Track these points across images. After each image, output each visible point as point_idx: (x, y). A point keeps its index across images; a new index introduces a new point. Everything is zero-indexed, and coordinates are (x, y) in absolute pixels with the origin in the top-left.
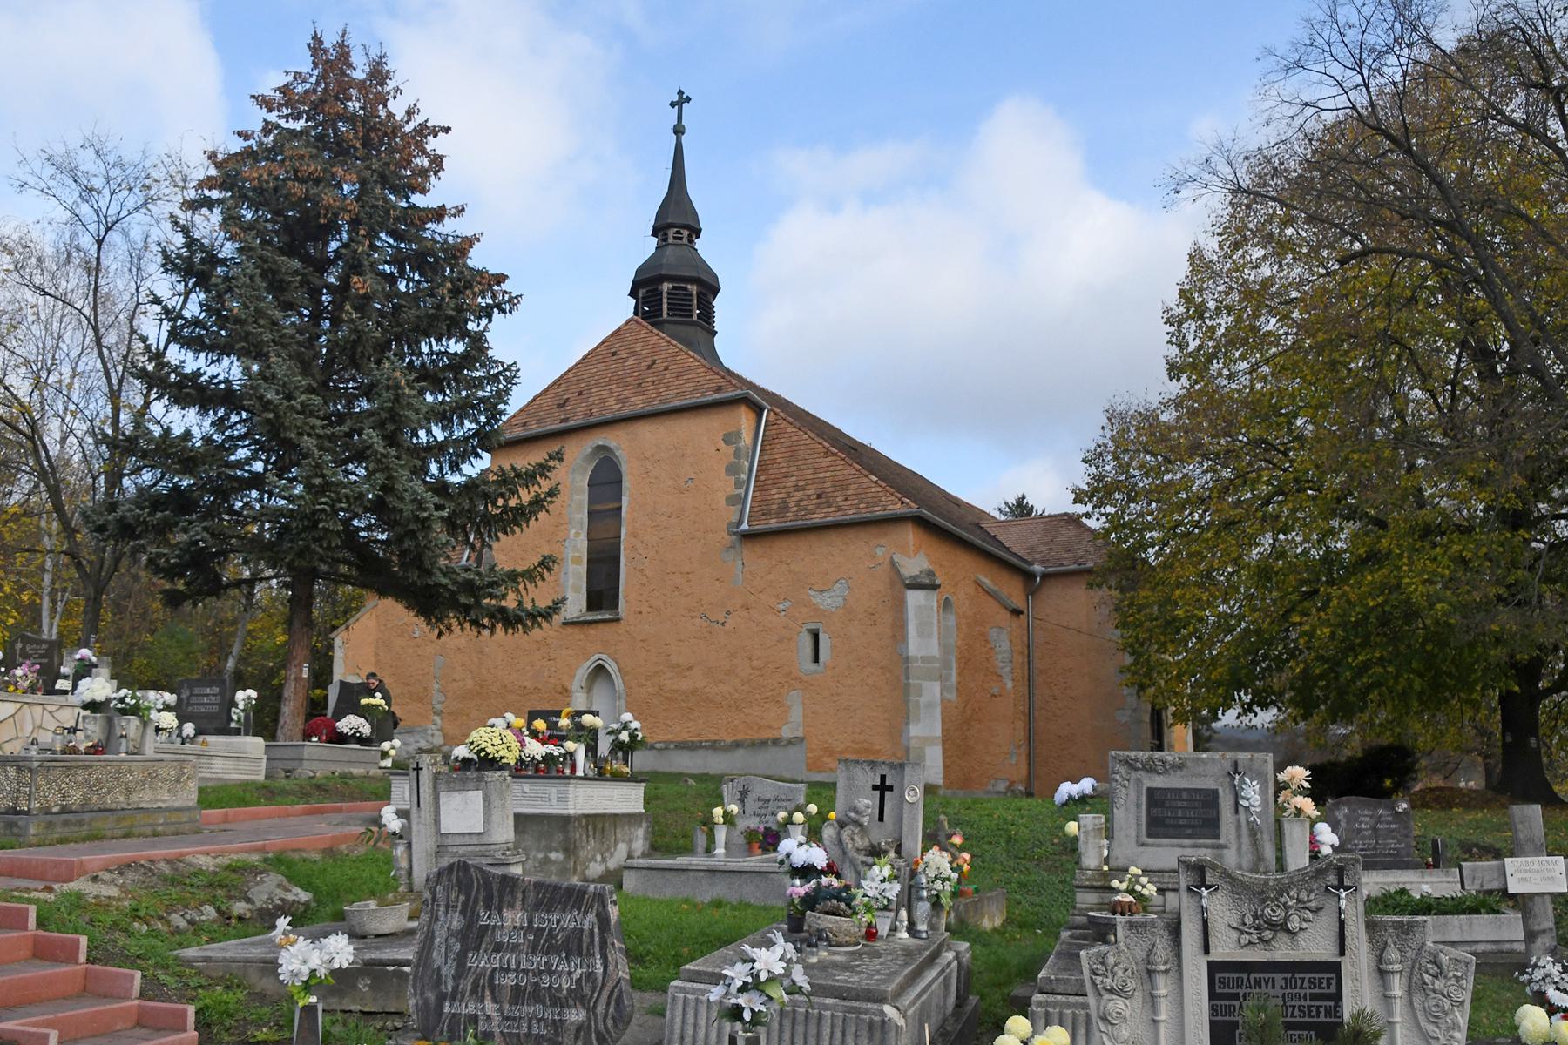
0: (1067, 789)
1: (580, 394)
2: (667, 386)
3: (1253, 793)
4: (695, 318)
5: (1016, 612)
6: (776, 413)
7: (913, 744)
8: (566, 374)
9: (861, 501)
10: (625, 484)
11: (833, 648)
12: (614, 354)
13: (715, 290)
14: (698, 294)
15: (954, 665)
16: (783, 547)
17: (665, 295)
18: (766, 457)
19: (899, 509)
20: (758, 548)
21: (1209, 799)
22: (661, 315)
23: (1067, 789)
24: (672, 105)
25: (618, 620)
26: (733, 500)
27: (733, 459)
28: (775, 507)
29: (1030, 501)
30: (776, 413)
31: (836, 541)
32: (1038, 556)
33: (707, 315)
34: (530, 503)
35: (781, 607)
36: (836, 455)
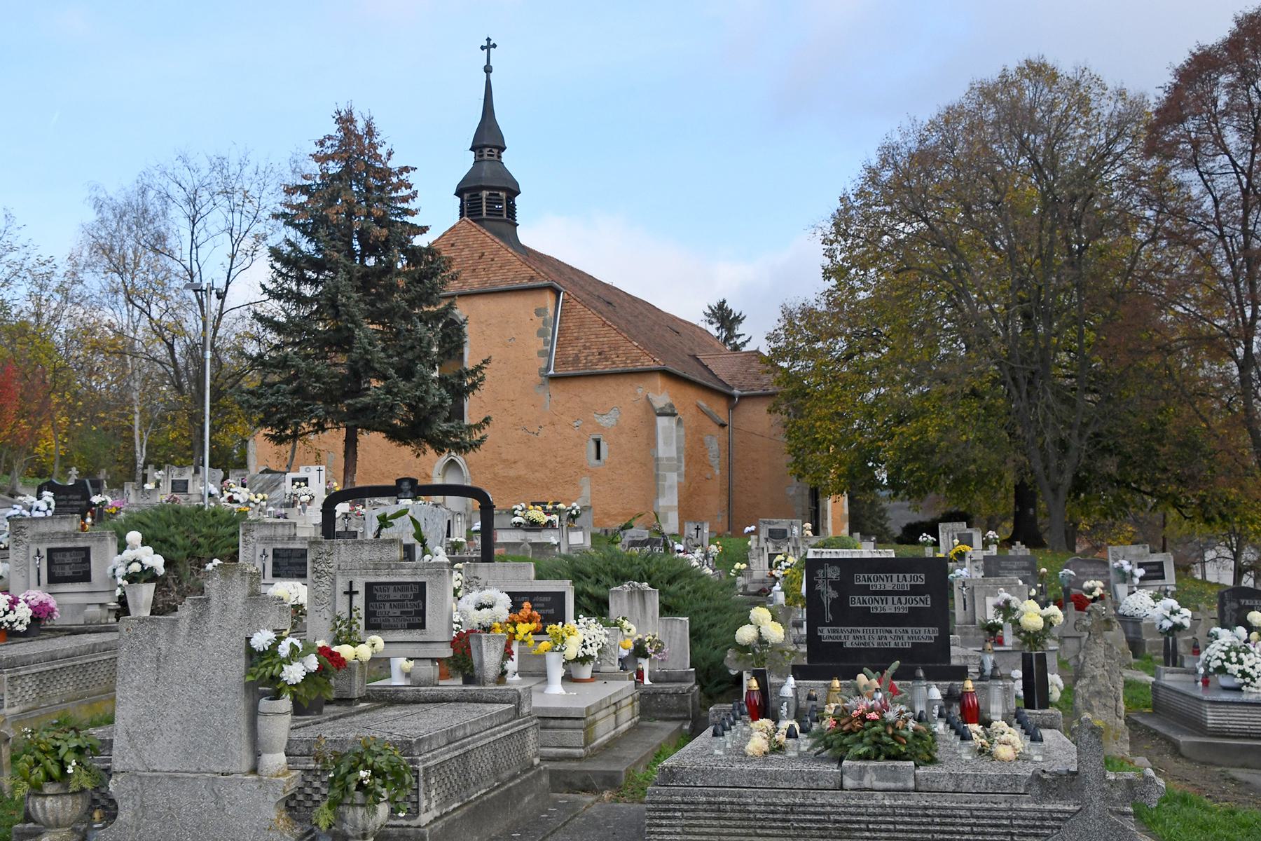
0: (748, 529)
3: (796, 530)
4: (505, 216)
5: (723, 425)
7: (661, 510)
9: (627, 359)
11: (610, 450)
12: (453, 245)
15: (683, 460)
16: (576, 386)
17: (484, 200)
19: (653, 365)
20: (560, 386)
21: (785, 532)
23: (748, 529)
26: (541, 353)
29: (729, 305)
31: (611, 384)
32: (736, 383)
33: (511, 211)
35: (576, 424)
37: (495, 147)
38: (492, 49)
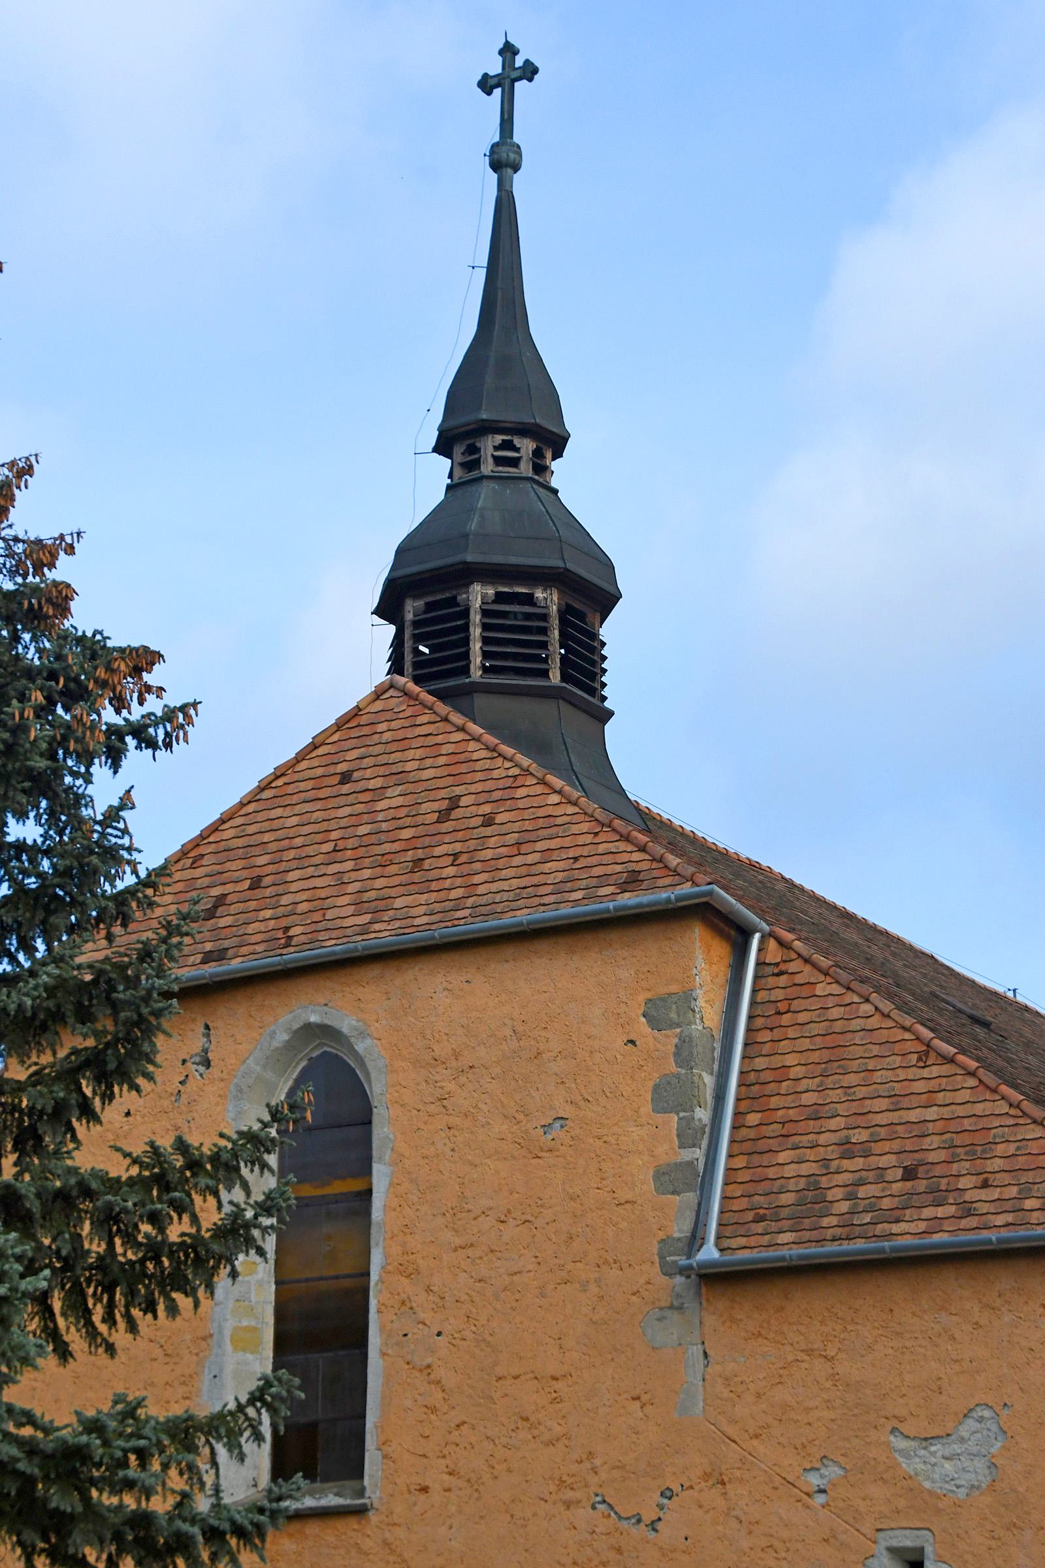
1: (256, 884)
2: (493, 868)
4: (555, 677)
6: (781, 943)
8: (215, 828)
10: (382, 1131)
12: (346, 778)
13: (607, 600)
14: (566, 613)
17: (476, 618)
18: (760, 1063)
22: (466, 671)
24: (486, 85)
25: (360, 1511)
27: (672, 1067)
28: (787, 1198)
30: (781, 943)
34: (220, 1232)
35: (814, 1480)
36: (951, 1060)
37: (524, 431)
38: (521, 87)
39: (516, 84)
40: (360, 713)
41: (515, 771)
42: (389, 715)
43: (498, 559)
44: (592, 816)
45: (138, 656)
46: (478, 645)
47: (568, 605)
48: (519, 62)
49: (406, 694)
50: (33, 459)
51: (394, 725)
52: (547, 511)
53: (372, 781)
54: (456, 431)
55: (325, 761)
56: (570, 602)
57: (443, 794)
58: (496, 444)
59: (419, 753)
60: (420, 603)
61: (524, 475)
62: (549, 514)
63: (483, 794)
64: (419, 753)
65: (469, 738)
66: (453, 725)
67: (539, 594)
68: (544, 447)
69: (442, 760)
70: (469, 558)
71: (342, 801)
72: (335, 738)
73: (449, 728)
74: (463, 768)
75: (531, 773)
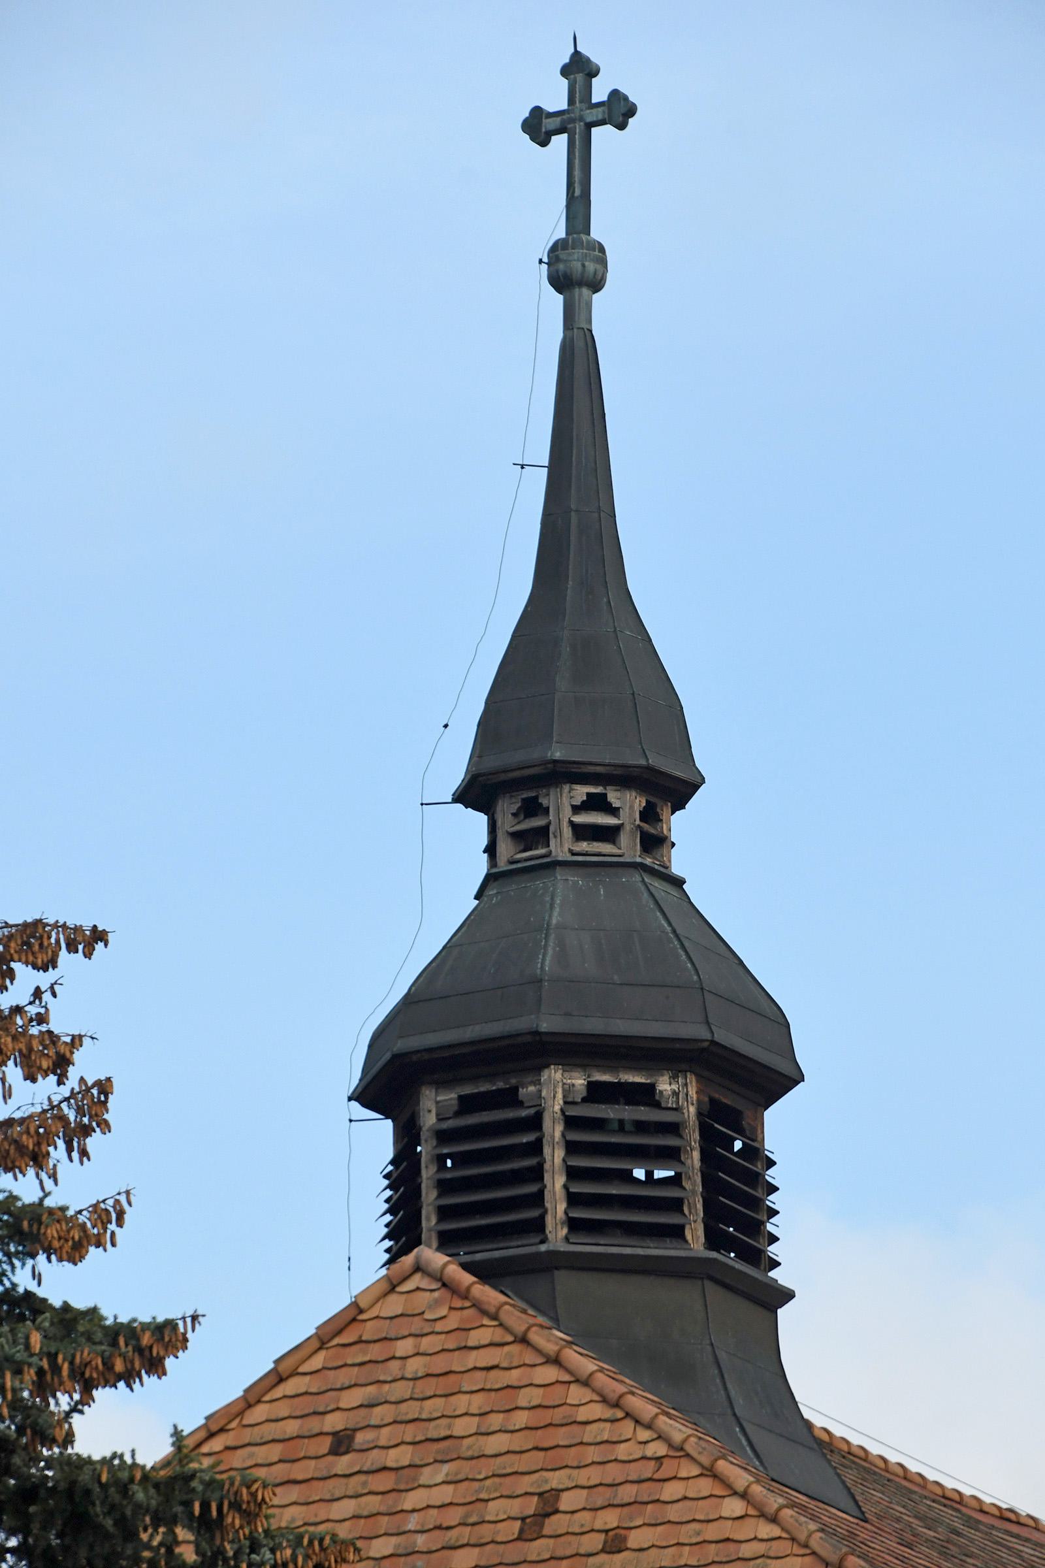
12: (342, 1443)
17: (554, 1130)
22: (538, 1226)
37: (626, 779)
38: (601, 135)
39: (595, 131)
40: (361, 1317)
41: (658, 1448)
42: (416, 1325)
43: (593, 1025)
44: (806, 1546)
45: (323, 1549)
46: (560, 1180)
47: (712, 1101)
48: (600, 93)
49: (444, 1285)
50: (123, 1199)
51: (426, 1343)
52: (674, 931)
53: (392, 1452)
54: (503, 777)
55: (305, 1405)
56: (717, 1096)
57: (526, 1484)
58: (577, 801)
59: (477, 1403)
60: (450, 1097)
61: (627, 859)
62: (677, 936)
63: (600, 1489)
64: (477, 1403)
65: (567, 1378)
66: (539, 1351)
67: (665, 1085)
68: (659, 803)
69: (521, 1419)
70: (545, 1026)
71: (336, 1487)
72: (317, 1362)
73: (530, 1357)
74: (561, 1436)
75: (688, 1455)
